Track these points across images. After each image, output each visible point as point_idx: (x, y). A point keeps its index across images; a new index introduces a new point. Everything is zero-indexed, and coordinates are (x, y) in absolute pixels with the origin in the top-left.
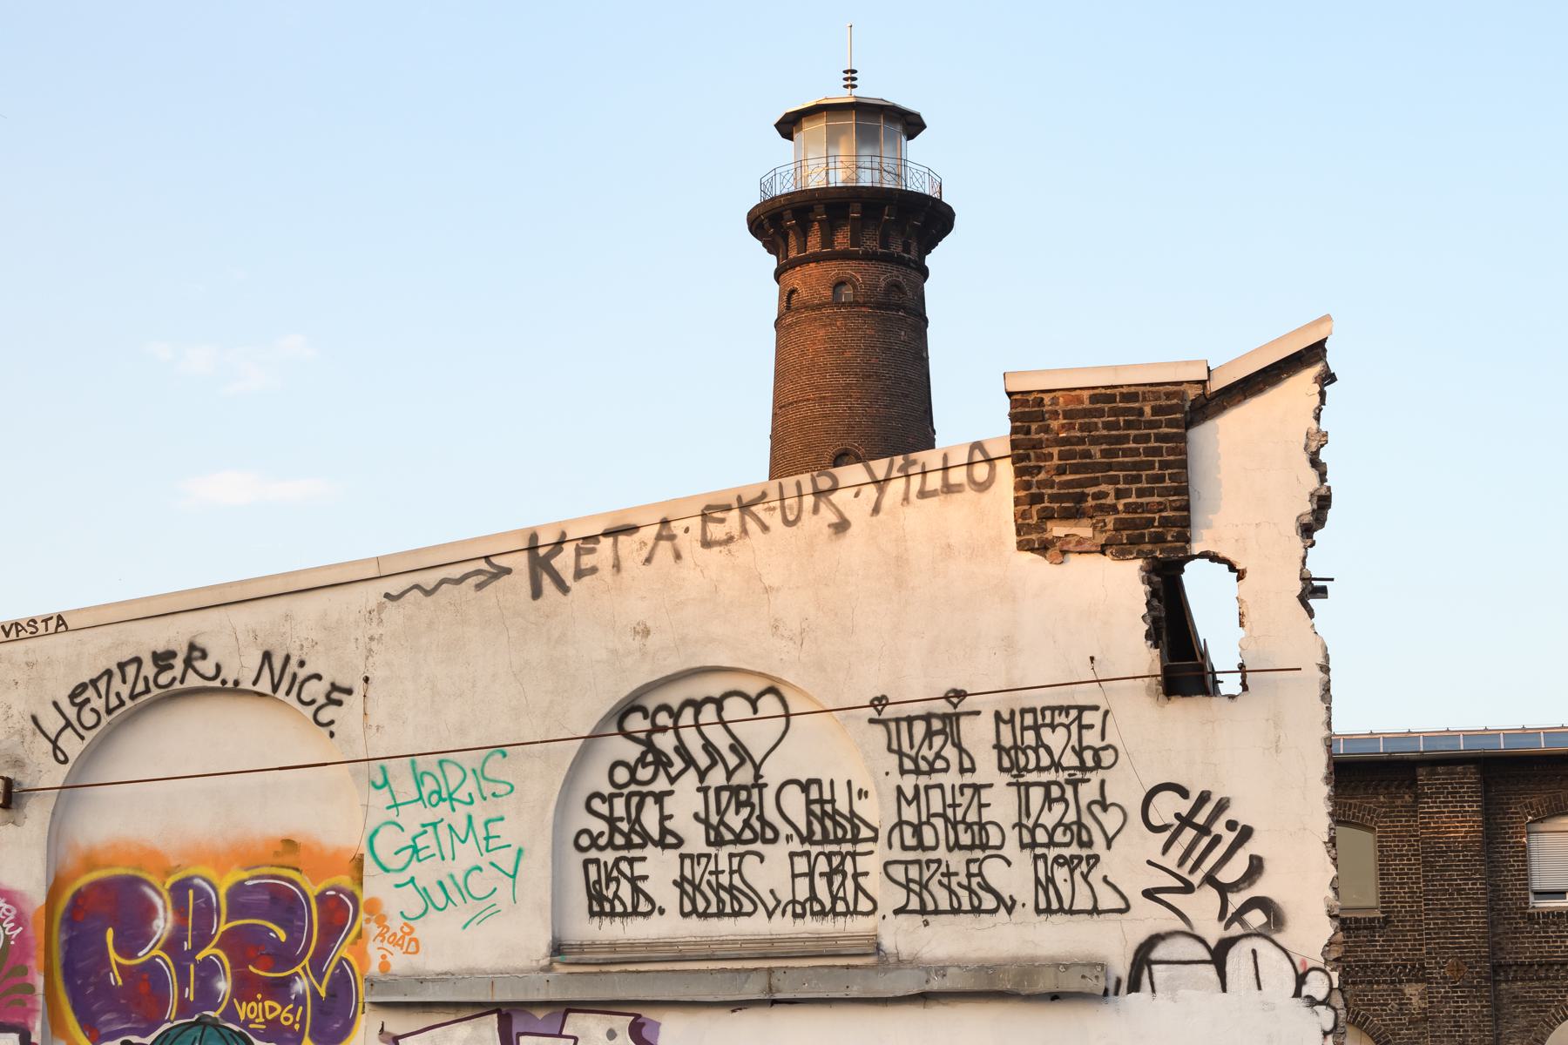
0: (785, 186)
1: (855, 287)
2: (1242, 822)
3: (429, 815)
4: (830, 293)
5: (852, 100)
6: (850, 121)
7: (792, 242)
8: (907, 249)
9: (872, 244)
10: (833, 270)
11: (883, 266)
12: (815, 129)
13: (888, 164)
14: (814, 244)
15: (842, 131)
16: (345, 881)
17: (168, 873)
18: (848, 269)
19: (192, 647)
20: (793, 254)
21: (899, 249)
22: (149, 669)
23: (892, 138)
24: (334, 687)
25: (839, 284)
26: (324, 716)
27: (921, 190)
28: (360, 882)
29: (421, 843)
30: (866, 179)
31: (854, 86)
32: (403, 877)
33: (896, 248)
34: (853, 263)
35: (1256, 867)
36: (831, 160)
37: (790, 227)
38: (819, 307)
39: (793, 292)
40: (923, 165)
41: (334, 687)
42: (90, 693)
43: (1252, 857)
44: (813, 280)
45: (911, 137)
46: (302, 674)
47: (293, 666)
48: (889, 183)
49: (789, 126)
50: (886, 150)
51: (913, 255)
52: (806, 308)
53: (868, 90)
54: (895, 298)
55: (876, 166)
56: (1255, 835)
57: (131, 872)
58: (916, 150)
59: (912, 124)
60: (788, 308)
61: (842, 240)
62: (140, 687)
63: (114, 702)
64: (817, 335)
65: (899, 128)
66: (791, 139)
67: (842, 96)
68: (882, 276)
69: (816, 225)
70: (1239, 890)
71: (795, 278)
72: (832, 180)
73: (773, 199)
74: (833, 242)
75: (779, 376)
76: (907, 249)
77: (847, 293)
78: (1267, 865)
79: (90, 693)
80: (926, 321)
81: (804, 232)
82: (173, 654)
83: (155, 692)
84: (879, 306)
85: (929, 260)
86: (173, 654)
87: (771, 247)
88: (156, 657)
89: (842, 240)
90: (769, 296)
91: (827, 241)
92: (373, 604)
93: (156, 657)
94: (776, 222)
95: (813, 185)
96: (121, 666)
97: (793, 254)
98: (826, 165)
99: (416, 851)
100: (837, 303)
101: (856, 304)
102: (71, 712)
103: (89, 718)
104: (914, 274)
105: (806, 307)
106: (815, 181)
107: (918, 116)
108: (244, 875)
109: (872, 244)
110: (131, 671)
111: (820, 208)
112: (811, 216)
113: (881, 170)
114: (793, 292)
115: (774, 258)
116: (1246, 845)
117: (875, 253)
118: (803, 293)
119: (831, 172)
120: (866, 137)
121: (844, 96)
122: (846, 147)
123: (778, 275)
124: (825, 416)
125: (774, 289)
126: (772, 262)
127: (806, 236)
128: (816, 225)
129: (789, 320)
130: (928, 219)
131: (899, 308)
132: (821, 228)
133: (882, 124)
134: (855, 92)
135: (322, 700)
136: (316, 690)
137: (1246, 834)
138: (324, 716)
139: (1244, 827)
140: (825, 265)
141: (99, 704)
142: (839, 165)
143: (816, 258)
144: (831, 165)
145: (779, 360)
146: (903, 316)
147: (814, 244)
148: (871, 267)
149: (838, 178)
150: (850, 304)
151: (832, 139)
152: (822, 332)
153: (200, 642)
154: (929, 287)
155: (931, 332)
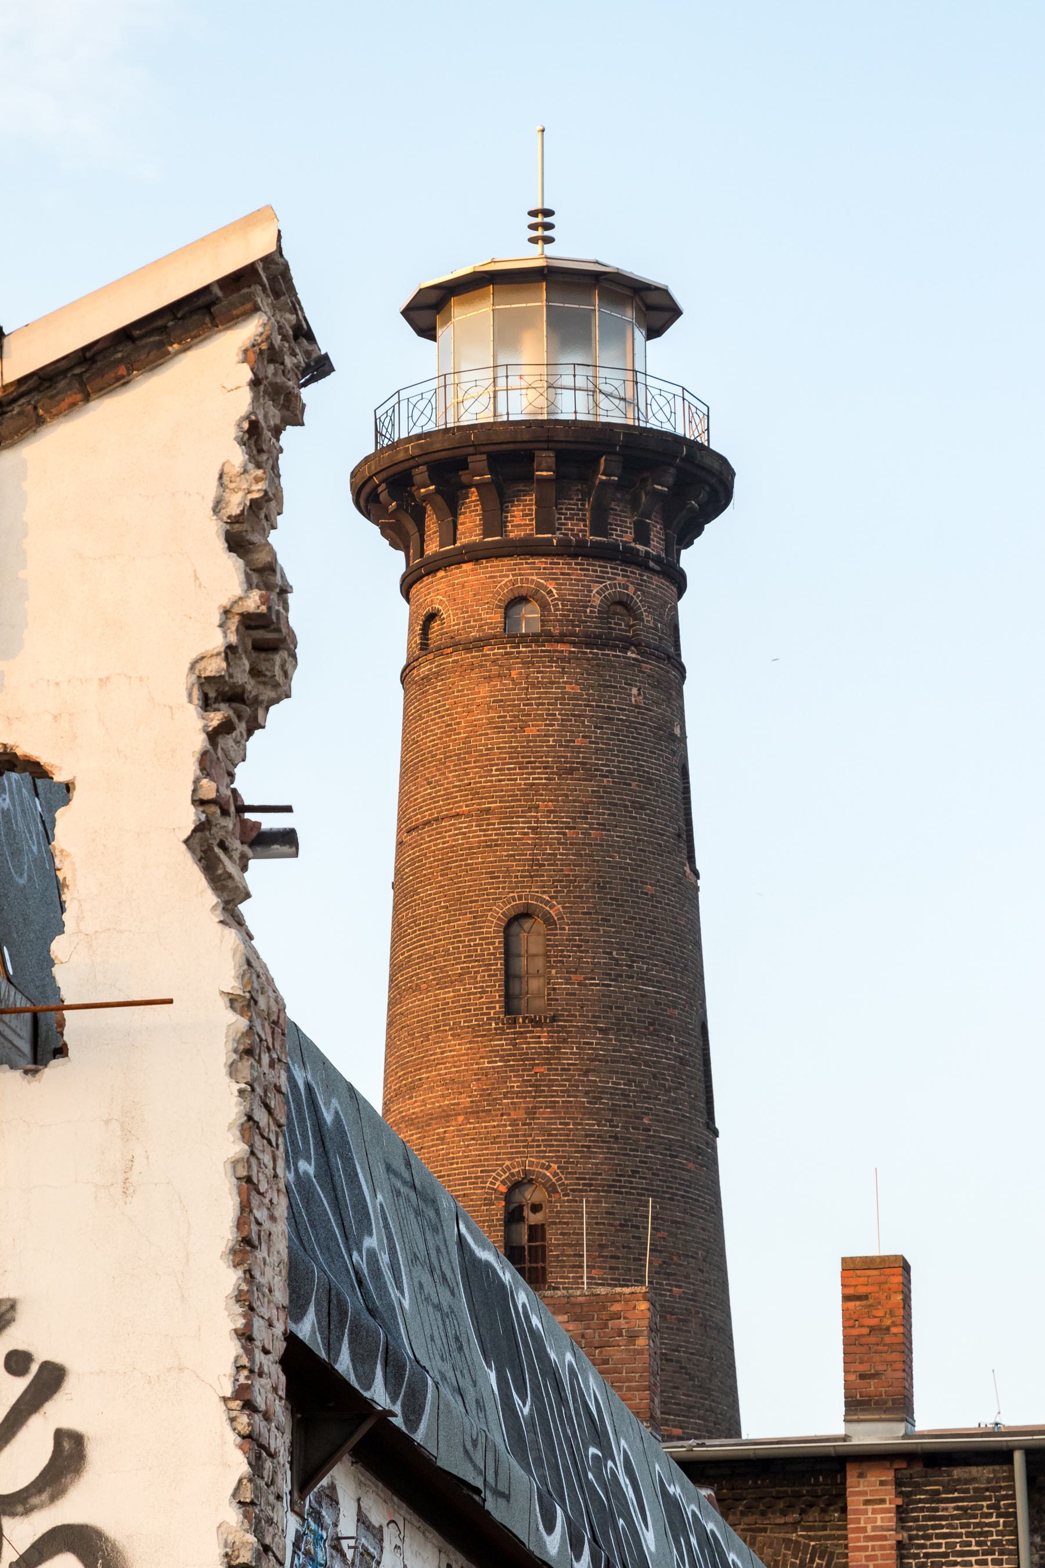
0: (419, 420)
1: (544, 606)
2: (41, 1356)
4: (497, 617)
5: (541, 263)
6: (536, 303)
7: (432, 524)
8: (642, 535)
9: (576, 526)
10: (504, 575)
11: (596, 567)
12: (471, 318)
13: (612, 380)
14: (470, 527)
15: (524, 320)
18: (533, 574)
20: (432, 547)
21: (629, 537)
23: (616, 335)
25: (518, 600)
27: (667, 427)
30: (572, 407)
31: (549, 240)
33: (624, 535)
34: (540, 562)
35: (69, 1455)
36: (501, 372)
37: (426, 498)
39: (431, 617)
40: (670, 385)
43: (60, 1435)
44: (470, 595)
45: (654, 332)
48: (612, 413)
50: (606, 356)
51: (656, 546)
53: (573, 246)
54: (620, 626)
55: (581, 382)
56: (70, 1385)
58: (661, 356)
60: (424, 646)
61: (521, 520)
64: (475, 694)
65: (629, 315)
66: (433, 338)
67: (527, 255)
69: (474, 495)
70: (27, 1512)
71: (436, 591)
72: (502, 409)
73: (394, 446)
74: (503, 524)
75: (409, 771)
76: (642, 535)
77: (530, 617)
78: (93, 1452)
80: (682, 671)
81: (452, 504)
84: (590, 641)
85: (688, 560)
87: (397, 535)
89: (521, 520)
91: (494, 522)
95: (467, 420)
97: (432, 547)
98: (501, 379)
100: (511, 637)
101: (543, 637)
104: (657, 583)
105: (456, 645)
106: (475, 412)
107: (664, 292)
109: (576, 526)
111: (478, 461)
112: (464, 477)
113: (594, 391)
114: (431, 617)
115: (401, 555)
116: (49, 1407)
117: (581, 544)
118: (451, 620)
119: (502, 396)
120: (569, 332)
121: (531, 256)
122: (533, 347)
123: (407, 587)
124: (490, 845)
125: (399, 615)
126: (397, 562)
127: (454, 513)
128: (474, 495)
129: (424, 670)
131: (628, 643)
132: (482, 499)
133: (597, 309)
134: (550, 250)
137: (50, 1380)
139: (46, 1365)
140: (489, 567)
142: (514, 382)
143: (474, 555)
144: (501, 383)
145: (409, 744)
146: (632, 659)
147: (470, 527)
148: (573, 570)
149: (520, 405)
150: (535, 638)
151: (505, 336)
152: (484, 690)
155: (690, 689)
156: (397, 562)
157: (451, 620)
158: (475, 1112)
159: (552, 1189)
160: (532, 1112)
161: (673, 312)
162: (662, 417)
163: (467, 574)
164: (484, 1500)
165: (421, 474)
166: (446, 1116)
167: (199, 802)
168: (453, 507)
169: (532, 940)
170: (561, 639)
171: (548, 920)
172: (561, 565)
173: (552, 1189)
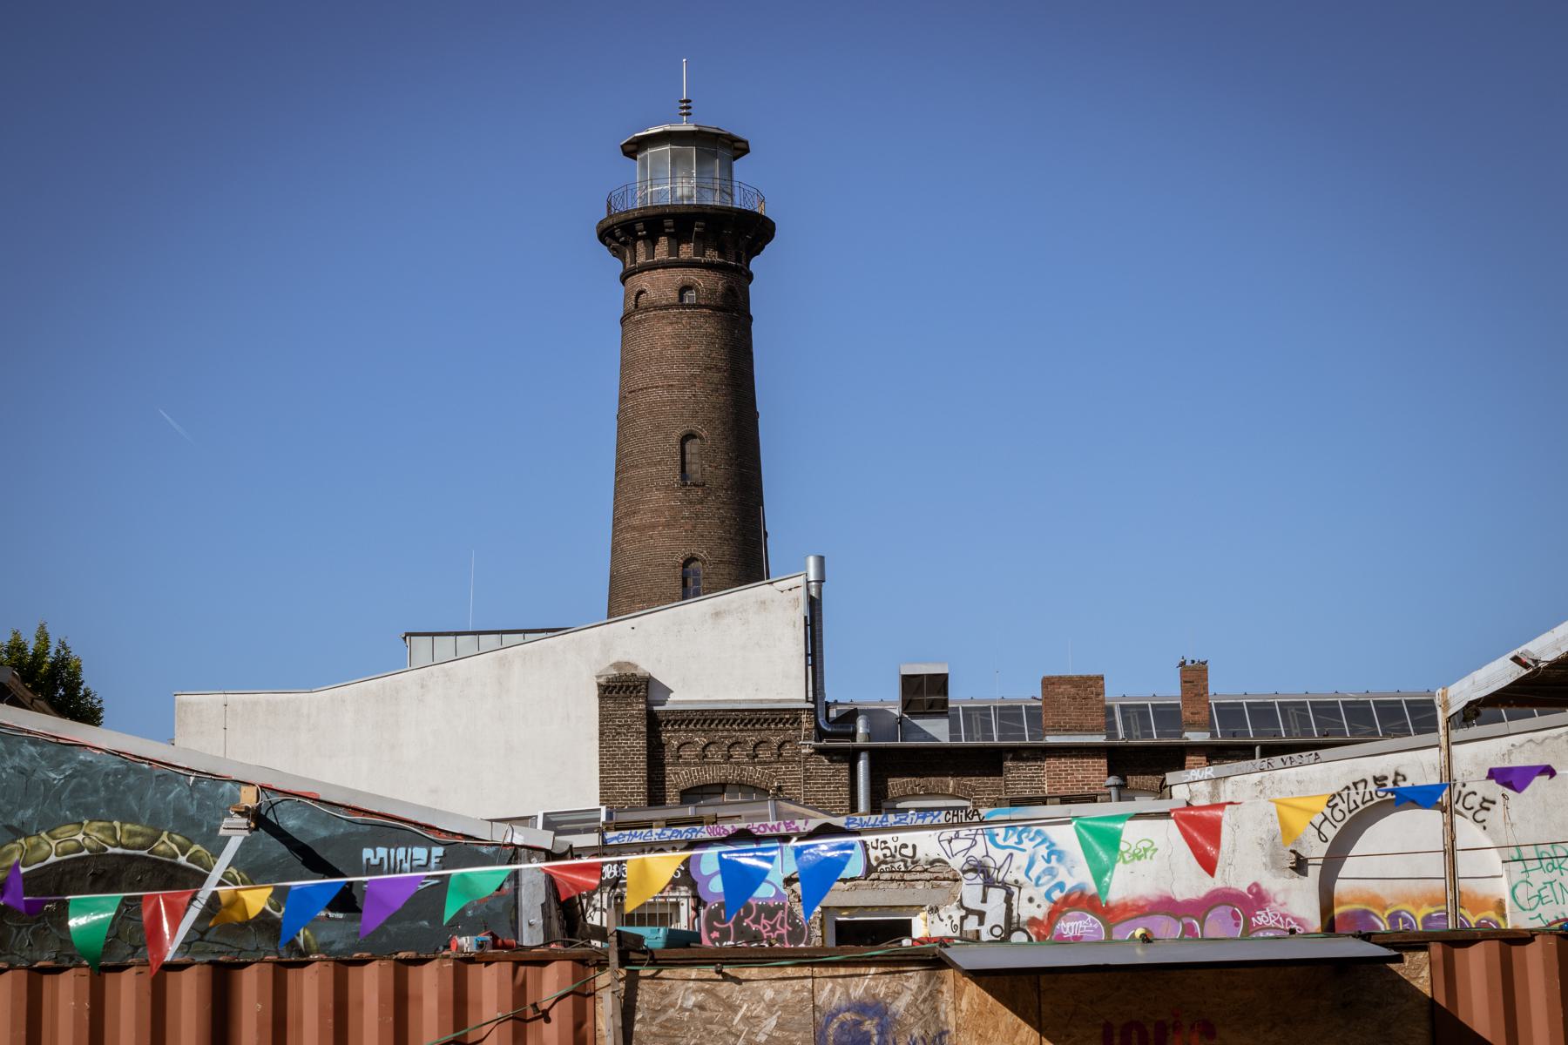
3: (1547, 877)
4: (675, 295)
7: (640, 246)
10: (679, 276)
16: (1492, 915)
17: (1385, 908)
18: (692, 275)
19: (1397, 774)
20: (641, 259)
22: (1372, 787)
24: (1485, 800)
25: (684, 289)
26: (1479, 817)
28: (1504, 916)
29: (1543, 893)
32: (1534, 914)
38: (667, 307)
40: (751, 185)
41: (1485, 800)
42: (1338, 800)
44: (659, 285)
46: (1465, 791)
47: (1459, 787)
49: (634, 148)
52: (656, 308)
57: (1363, 907)
58: (737, 164)
59: (736, 147)
62: (1368, 797)
63: (1353, 806)
68: (703, 281)
71: (643, 281)
77: (690, 297)
79: (1338, 800)
80: (750, 318)
81: (652, 240)
82: (1386, 778)
83: (1377, 800)
86: (1386, 778)
87: (617, 253)
88: (1376, 779)
90: (615, 298)
91: (674, 251)
92: (1504, 750)
93: (1376, 779)
94: (625, 233)
96: (1355, 784)
97: (641, 259)
98: (671, 184)
99: (1541, 898)
102: (1328, 812)
103: (1339, 816)
108: (1432, 910)
110: (1361, 786)
115: (619, 263)
123: (624, 279)
124: (673, 401)
126: (617, 266)
130: (735, 236)
135: (1477, 807)
136: (1473, 801)
138: (1479, 817)
141: (1343, 806)
143: (665, 266)
146: (733, 314)
147: (662, 250)
150: (689, 306)
152: (669, 329)
153: (1401, 771)
154: (753, 288)
156: (617, 266)
157: (652, 294)
158: (667, 525)
159: (704, 562)
160: (694, 527)
161: (746, 151)
162: (738, 203)
163: (659, 274)
164: (789, 881)
165: (639, 226)
166: (653, 526)
167: (850, 716)
168: (655, 243)
169: (692, 447)
170: (705, 306)
171: (701, 438)
172: (705, 272)
173: (704, 562)
